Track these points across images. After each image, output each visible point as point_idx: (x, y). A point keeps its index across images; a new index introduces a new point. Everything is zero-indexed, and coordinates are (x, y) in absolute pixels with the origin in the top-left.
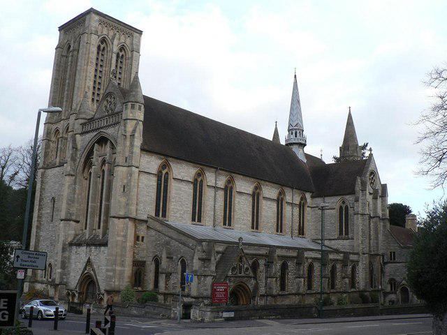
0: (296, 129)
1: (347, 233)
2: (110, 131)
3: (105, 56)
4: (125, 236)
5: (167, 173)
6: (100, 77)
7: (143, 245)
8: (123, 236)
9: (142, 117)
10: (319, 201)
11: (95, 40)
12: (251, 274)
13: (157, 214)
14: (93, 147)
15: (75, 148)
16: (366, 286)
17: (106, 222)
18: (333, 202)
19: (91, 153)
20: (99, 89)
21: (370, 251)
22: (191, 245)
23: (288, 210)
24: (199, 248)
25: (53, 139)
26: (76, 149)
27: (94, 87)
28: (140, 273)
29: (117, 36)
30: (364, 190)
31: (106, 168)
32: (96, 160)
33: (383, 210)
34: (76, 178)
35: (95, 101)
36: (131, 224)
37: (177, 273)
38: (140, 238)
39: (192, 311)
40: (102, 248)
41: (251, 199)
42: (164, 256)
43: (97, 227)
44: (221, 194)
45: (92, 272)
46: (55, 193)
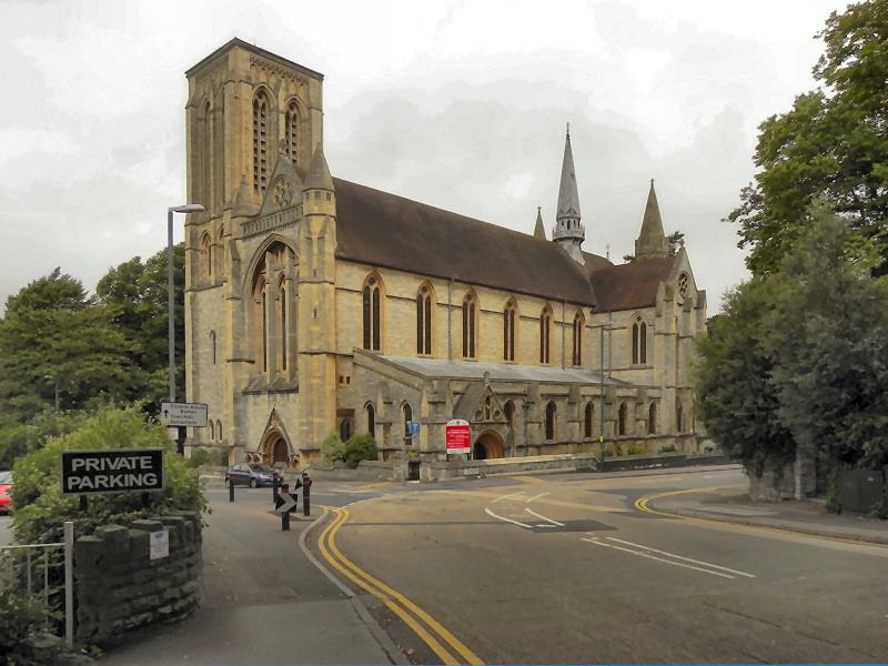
0: (569, 214)
1: (643, 361)
2: (287, 234)
3: (267, 117)
4: (322, 378)
5: (377, 289)
6: (263, 152)
7: (350, 388)
8: (319, 378)
9: (333, 213)
10: (603, 318)
11: (248, 93)
12: (504, 420)
13: (367, 345)
14: (265, 253)
15: (236, 259)
16: (670, 430)
17: (294, 360)
18: (624, 319)
19: (261, 266)
20: (263, 170)
21: (677, 383)
22: (416, 385)
23: (556, 333)
24: (428, 388)
25: (202, 247)
26: (239, 260)
27: (256, 168)
28: (348, 425)
29: (283, 84)
30: (669, 300)
31: (286, 285)
32: (269, 274)
33: (698, 327)
34: (243, 303)
35: (260, 189)
36: (329, 363)
37: (399, 422)
38: (345, 379)
39: (421, 470)
40: (292, 395)
41: (502, 319)
42: (380, 402)
43: (281, 368)
44: (458, 314)
45: (279, 428)
46: (214, 324)
